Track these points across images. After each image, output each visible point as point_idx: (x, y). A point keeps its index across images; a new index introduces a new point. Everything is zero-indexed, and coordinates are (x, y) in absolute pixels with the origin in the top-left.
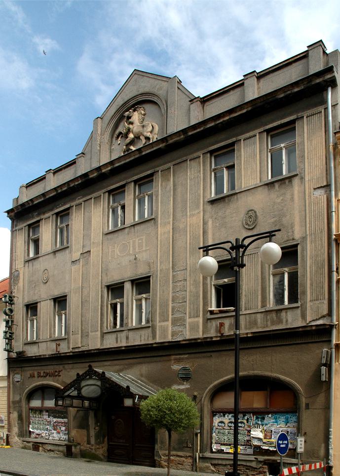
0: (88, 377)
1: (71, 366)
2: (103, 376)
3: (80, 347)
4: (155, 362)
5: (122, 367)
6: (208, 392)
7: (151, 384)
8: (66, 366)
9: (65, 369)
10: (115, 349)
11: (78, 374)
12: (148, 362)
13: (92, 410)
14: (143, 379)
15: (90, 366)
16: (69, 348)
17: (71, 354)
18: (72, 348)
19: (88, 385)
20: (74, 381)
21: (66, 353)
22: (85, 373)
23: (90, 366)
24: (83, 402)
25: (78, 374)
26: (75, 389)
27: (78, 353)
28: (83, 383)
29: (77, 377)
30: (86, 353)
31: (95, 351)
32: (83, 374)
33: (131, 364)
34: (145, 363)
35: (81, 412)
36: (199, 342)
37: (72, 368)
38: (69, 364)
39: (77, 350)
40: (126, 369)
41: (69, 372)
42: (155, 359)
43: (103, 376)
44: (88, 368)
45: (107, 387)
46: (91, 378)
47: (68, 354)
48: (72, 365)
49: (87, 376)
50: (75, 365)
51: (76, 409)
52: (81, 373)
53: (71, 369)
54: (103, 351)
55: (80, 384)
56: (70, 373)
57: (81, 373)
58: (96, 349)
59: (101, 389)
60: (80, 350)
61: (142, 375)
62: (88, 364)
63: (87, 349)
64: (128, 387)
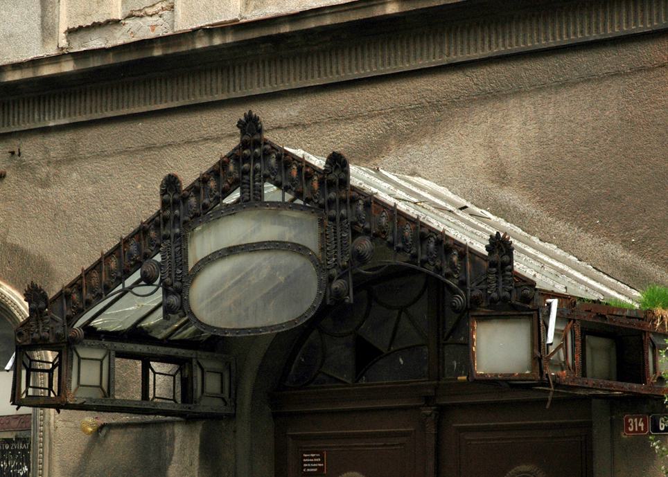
0: (236, 195)
1: (56, 145)
2: (331, 185)
3: (117, 22)
4: (188, 142)
5: (376, 126)
6: (603, 294)
7: (561, 227)
8: (31, 149)
9: (22, 167)
10: (339, 19)
11: (171, 183)
12: (540, 88)
13: (189, 418)
14: (509, 196)
15: (250, 126)
16: (47, 30)
17: (68, 67)
18: (71, 32)
19: (231, 251)
20: (142, 232)
21: (36, 63)
22: (218, 171)
23: (250, 126)
24: (146, 368)
25: (171, 183)
26: (147, 280)
27: (111, 60)
28: (203, 243)
29: (164, 204)
30: (157, 53)
31: (217, 41)
32: (203, 180)
33: (435, 106)
34: (518, 93)
35: (115, 438)
36: (158, 58)
37: (70, 159)
38: (46, 131)
39: (96, 42)
40: (403, 138)
41: (45, 184)
42: (583, 61)
43: (331, 185)
44: (235, 142)
45: (359, 257)
46: (252, 201)
47: (47, 71)
48: (68, 136)
49: (226, 193)
50: (90, 137)
51: (89, 420)
52: (187, 178)
53: (59, 163)
54: (266, 32)
55: (182, 241)
56: (54, 189)
57: (187, 178)
58: (222, 29)
59: (320, 267)
60: (120, 37)
61: (501, 176)
62: (240, 113)
63: (160, 32)
64: (500, 245)
